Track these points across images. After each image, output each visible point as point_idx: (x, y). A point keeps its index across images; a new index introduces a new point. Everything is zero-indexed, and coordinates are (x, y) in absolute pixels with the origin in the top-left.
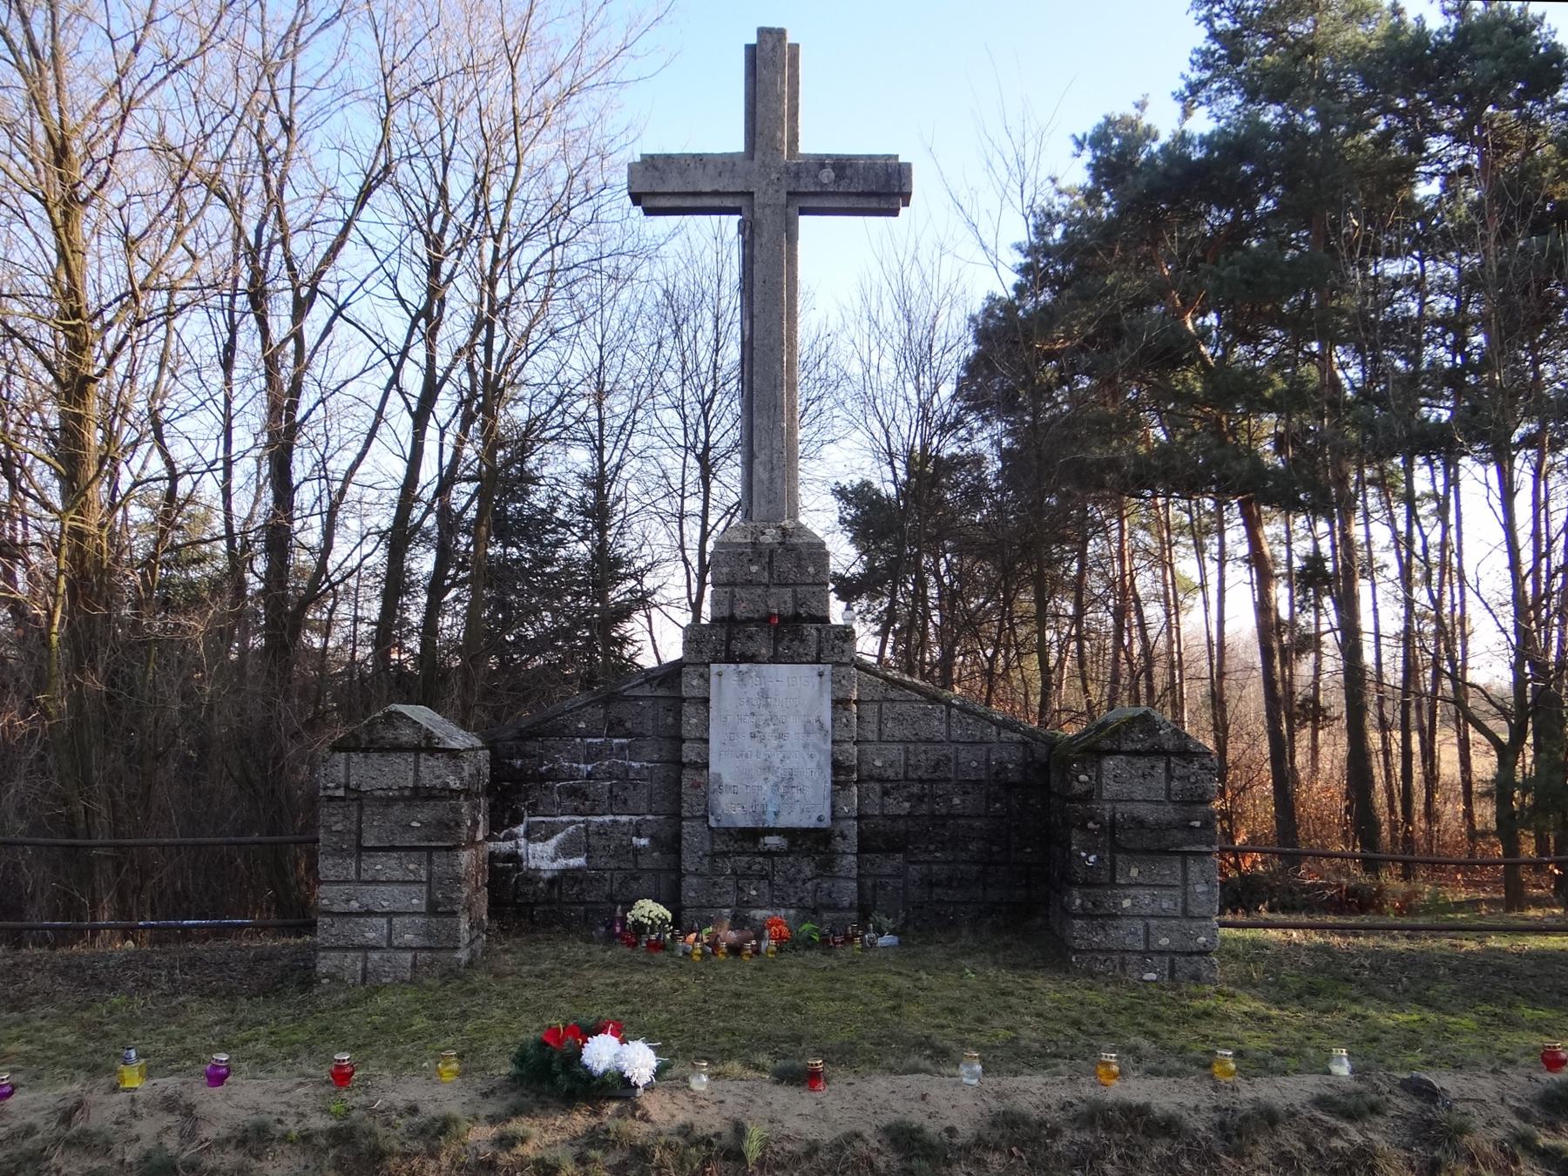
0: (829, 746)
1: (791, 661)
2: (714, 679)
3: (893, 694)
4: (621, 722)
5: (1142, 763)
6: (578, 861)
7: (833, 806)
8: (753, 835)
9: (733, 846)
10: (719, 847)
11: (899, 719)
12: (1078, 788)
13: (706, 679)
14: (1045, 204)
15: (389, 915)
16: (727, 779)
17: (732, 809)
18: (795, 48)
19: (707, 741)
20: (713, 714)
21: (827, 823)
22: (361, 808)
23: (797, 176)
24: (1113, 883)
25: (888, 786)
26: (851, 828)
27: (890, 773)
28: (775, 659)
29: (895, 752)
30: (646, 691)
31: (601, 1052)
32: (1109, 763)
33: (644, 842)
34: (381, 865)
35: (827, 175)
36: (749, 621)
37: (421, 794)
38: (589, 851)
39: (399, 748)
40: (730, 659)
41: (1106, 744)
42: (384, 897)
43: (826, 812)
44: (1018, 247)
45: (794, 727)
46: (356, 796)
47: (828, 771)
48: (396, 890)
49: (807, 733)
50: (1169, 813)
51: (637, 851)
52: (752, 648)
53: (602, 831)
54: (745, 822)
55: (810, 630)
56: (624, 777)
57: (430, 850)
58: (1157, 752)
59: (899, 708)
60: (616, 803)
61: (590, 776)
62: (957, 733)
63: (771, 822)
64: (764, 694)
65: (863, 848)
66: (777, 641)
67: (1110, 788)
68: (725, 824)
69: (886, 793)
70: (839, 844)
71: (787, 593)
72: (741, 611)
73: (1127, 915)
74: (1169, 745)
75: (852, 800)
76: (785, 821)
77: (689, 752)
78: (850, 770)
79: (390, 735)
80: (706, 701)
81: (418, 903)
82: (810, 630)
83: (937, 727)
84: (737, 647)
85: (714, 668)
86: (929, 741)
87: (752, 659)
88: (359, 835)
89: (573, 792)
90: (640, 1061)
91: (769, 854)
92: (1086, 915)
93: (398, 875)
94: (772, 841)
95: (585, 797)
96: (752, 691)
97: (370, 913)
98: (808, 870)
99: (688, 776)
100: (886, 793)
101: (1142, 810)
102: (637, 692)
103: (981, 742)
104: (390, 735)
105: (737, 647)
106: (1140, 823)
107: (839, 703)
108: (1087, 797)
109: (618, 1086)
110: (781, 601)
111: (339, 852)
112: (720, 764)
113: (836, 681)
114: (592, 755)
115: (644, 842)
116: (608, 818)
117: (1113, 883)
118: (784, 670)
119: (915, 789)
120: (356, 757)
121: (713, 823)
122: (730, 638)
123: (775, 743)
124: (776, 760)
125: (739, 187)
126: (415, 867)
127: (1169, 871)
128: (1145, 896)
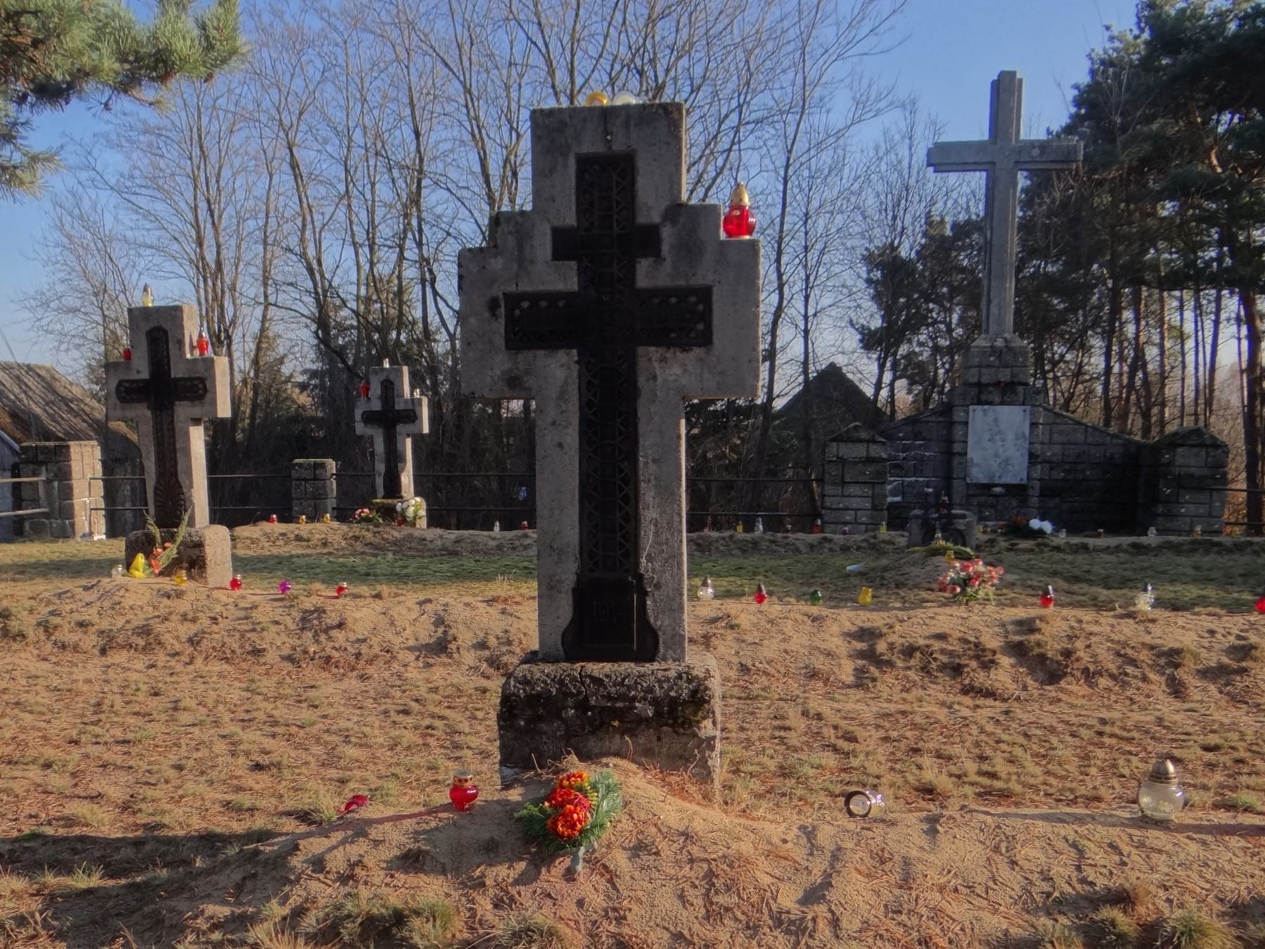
0: (1027, 445)
1: (1010, 404)
2: (971, 413)
3: (1058, 421)
4: (920, 433)
5: (1195, 450)
6: (898, 499)
7: (1028, 474)
8: (988, 487)
9: (978, 492)
10: (971, 492)
11: (1060, 433)
12: (1164, 461)
13: (967, 413)
14: (1101, 52)
15: (856, 510)
16: (976, 460)
17: (978, 475)
18: (1021, 81)
19: (966, 442)
20: (970, 429)
21: (1025, 482)
22: (843, 466)
23: (1020, 152)
24: (1177, 502)
25: (1052, 464)
26: (1037, 484)
27: (1054, 459)
28: (1002, 403)
29: (1057, 449)
30: (933, 418)
31: (1035, 524)
32: (1180, 450)
33: (930, 490)
34: (853, 490)
35: (1036, 152)
36: (988, 385)
37: (869, 460)
38: (903, 494)
39: (860, 441)
40: (980, 403)
41: (1179, 442)
42: (855, 503)
43: (1024, 476)
44: (1076, 87)
45: (1010, 436)
46: (841, 461)
47: (1026, 457)
48: (858, 500)
49: (1017, 439)
50: (1206, 472)
51: (927, 494)
52: (990, 398)
53: (910, 485)
54: (984, 480)
55: (1020, 389)
56: (921, 459)
57: (873, 484)
58: (1202, 445)
59: (1061, 427)
60: (917, 471)
61: (904, 459)
62: (1090, 440)
63: (997, 481)
64: (996, 420)
65: (1041, 495)
66: (1003, 394)
67: (1179, 461)
68: (975, 481)
69: (1052, 469)
70: (1031, 492)
71: (1008, 371)
72: (985, 380)
73: (1182, 515)
74: (1208, 442)
75: (1038, 472)
76: (1004, 481)
77: (957, 447)
78: (1038, 456)
79: (856, 435)
80: (967, 423)
81: (868, 505)
82: (1020, 389)
83: (1080, 437)
84: (984, 397)
85: (971, 407)
86: (1075, 444)
87: (991, 403)
88: (843, 477)
89: (896, 466)
90: (1047, 526)
91: (996, 496)
92: (1164, 515)
93: (860, 493)
94: (998, 490)
95: (902, 468)
96: (990, 418)
97: (847, 509)
98: (1014, 503)
99: (956, 460)
100: (1052, 469)
101: (1193, 470)
102: (929, 419)
103: (1103, 444)
104: (856, 435)
105: (984, 397)
106: (1192, 476)
107: (1034, 425)
108: (1170, 464)
109: (1041, 533)
110: (1004, 375)
111: (834, 484)
112: (972, 454)
113: (1032, 414)
114: (905, 449)
115: (930, 490)
116: (913, 479)
117: (1177, 502)
118: (1006, 408)
119: (1067, 467)
120: (842, 445)
121: (968, 480)
122: (980, 393)
123: (1000, 443)
124: (1001, 450)
125: (989, 159)
126: (867, 490)
127: (1204, 497)
128: (1192, 508)
